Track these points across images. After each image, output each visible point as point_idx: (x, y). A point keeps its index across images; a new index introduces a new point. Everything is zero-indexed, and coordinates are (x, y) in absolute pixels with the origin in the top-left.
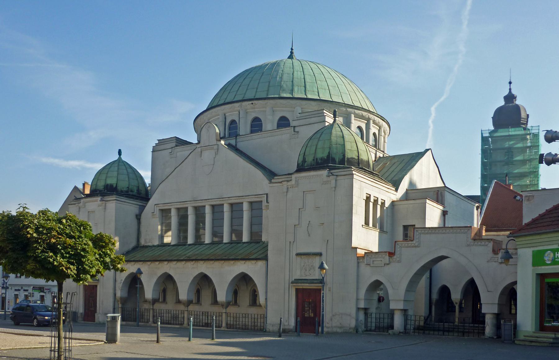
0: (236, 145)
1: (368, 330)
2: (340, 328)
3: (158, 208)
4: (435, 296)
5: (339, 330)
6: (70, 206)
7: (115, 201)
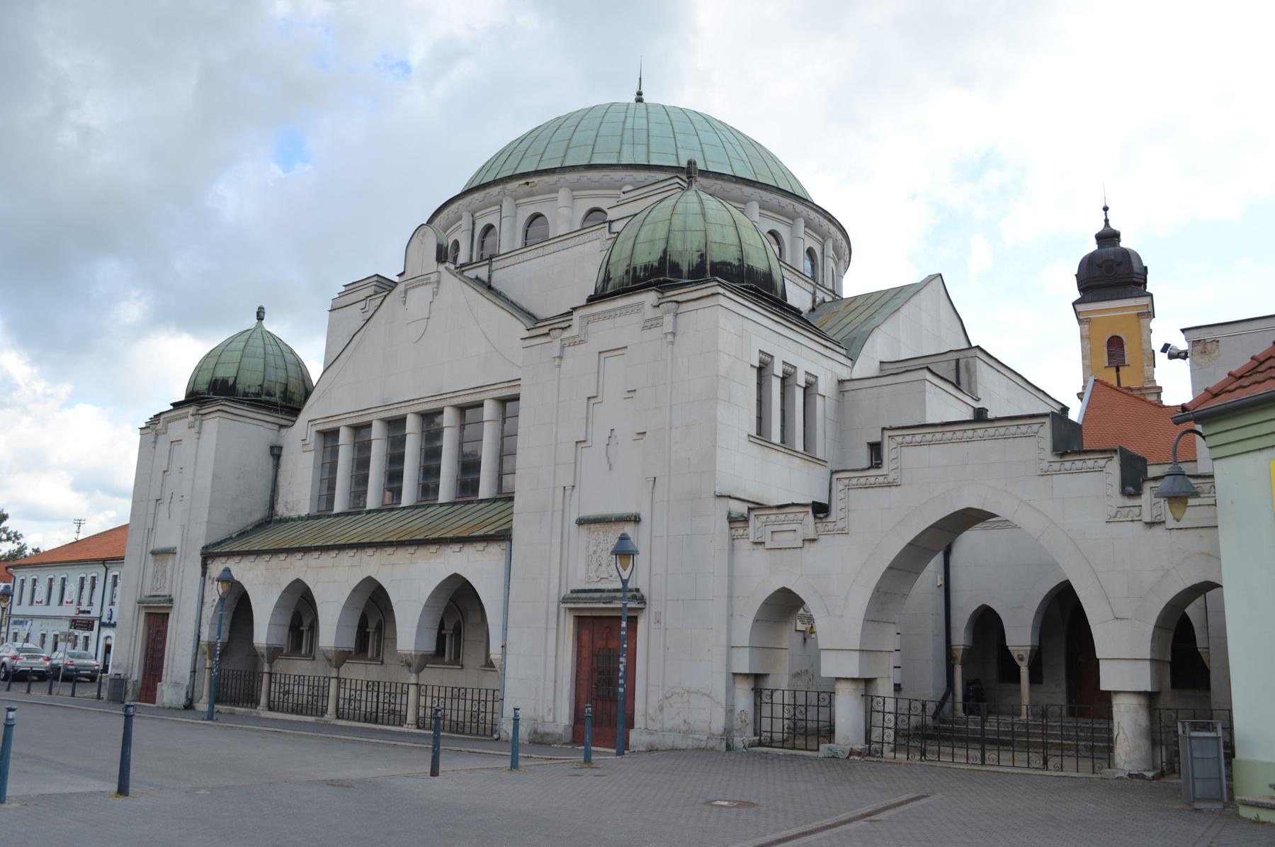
0: (490, 277)
1: (762, 741)
2: (687, 733)
3: (314, 429)
4: (961, 638)
5: (680, 743)
7: (219, 414)
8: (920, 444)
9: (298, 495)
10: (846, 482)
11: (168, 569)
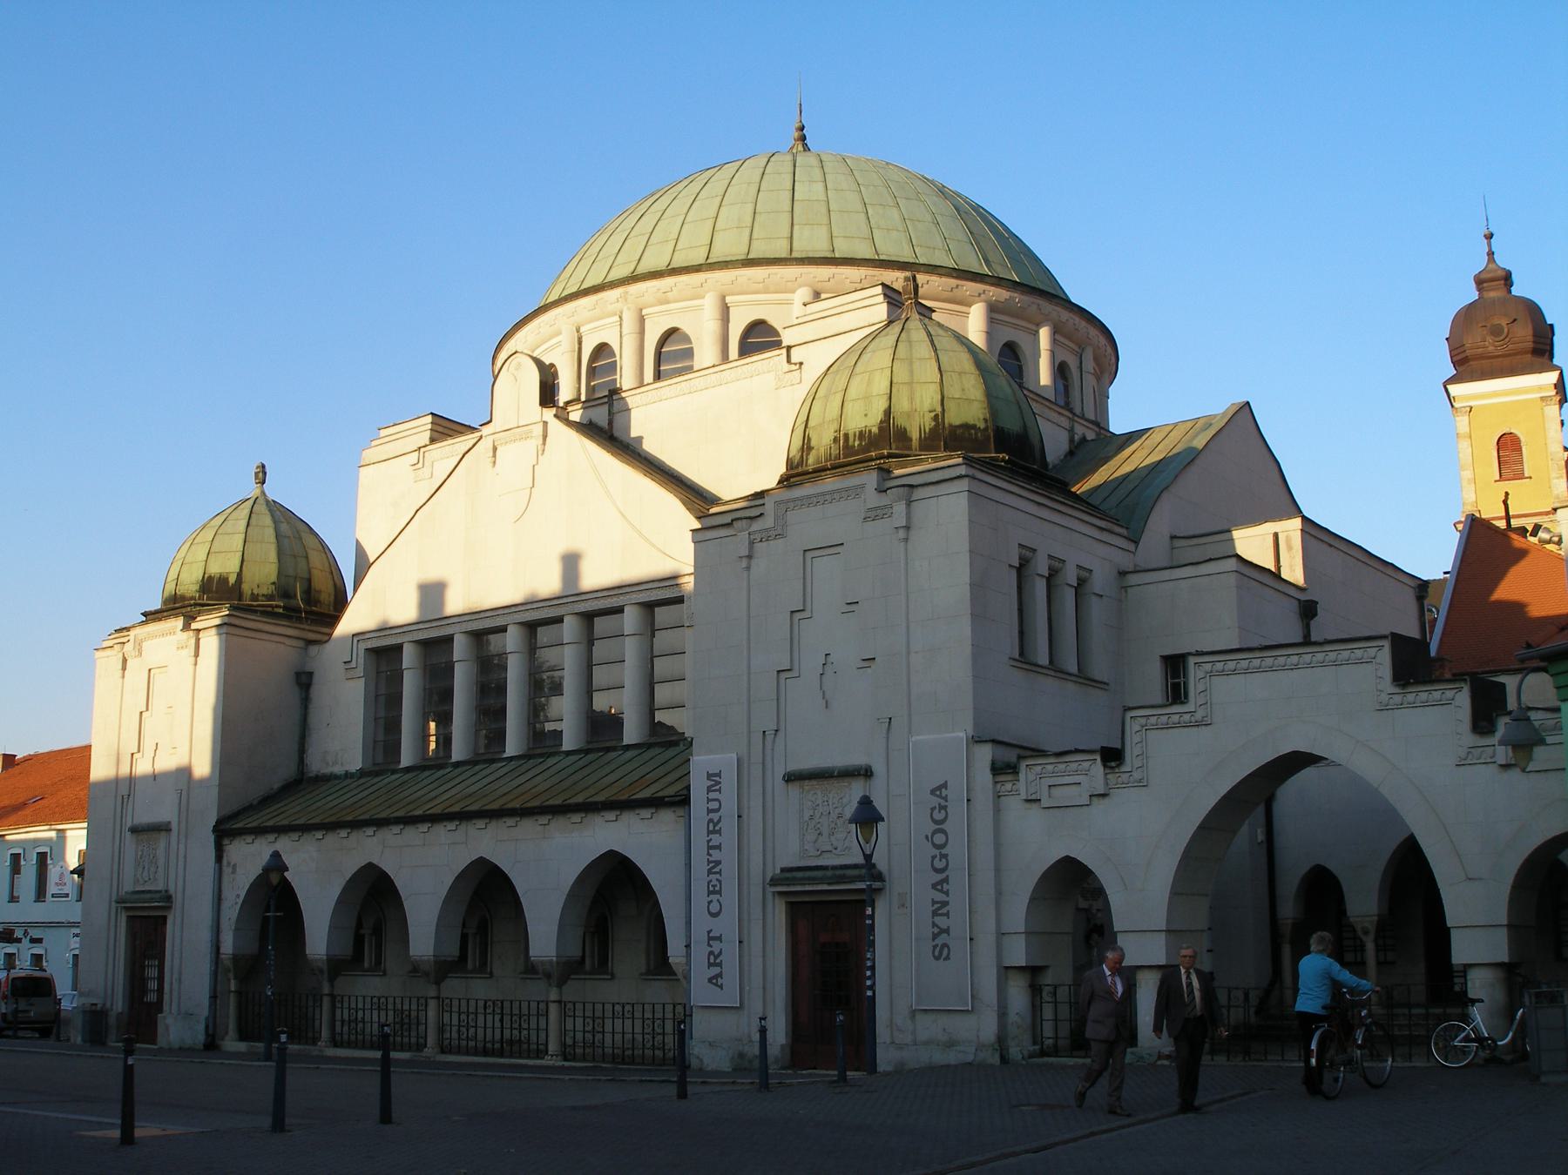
0: (611, 423)
3: (363, 646)
6: (98, 654)
8: (1234, 672)
9: (342, 739)
10: (1143, 721)
11: (161, 852)
